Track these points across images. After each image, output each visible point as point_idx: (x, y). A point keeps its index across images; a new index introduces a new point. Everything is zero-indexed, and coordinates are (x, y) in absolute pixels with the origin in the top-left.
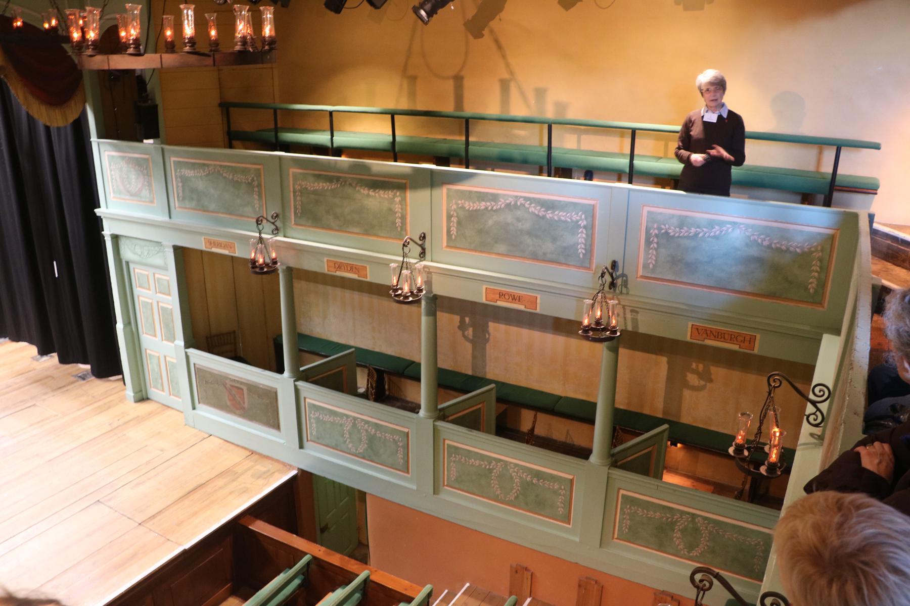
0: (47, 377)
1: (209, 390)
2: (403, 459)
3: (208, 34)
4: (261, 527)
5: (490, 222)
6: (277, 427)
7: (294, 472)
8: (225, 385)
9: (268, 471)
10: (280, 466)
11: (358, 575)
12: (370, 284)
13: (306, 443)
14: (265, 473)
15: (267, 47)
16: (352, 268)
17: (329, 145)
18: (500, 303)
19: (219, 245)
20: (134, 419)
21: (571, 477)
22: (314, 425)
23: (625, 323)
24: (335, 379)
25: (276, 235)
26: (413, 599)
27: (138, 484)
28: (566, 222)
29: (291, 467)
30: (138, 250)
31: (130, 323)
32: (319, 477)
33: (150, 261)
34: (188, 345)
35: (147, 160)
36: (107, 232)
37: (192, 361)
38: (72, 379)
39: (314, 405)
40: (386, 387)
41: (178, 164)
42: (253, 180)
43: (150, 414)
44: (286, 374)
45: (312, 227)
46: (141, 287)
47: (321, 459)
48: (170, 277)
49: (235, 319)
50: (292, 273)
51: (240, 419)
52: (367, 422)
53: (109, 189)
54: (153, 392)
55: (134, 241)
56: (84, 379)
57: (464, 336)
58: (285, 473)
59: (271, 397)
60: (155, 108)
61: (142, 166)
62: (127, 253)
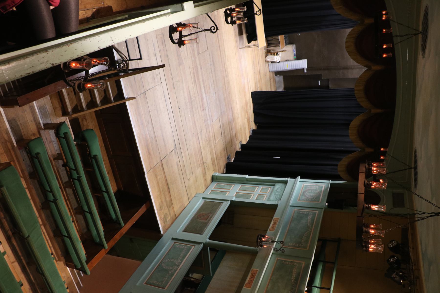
0: (232, 144)
1: (210, 206)
3: (373, 224)
4: (142, 210)
6: (185, 231)
7: (162, 232)
8: (210, 213)
9: (166, 222)
10: (167, 227)
11: (107, 243)
12: (242, 287)
13: (174, 241)
14: (166, 220)
15: (364, 244)
16: (251, 281)
17: (314, 285)
19: (274, 224)
20: (205, 172)
22: (181, 247)
24: (199, 264)
25: (274, 250)
26: (87, 264)
27: (178, 165)
29: (165, 232)
30: (279, 190)
31: (247, 181)
32: (157, 243)
33: (273, 194)
34: (232, 201)
35: (319, 201)
36: (289, 179)
37: (225, 202)
38: (229, 154)
39: (190, 249)
40: (189, 289)
41: (315, 213)
42: (302, 245)
43: (205, 180)
44: (208, 240)
45: (275, 266)
46: (262, 189)
47: (165, 245)
48: (264, 201)
49: (239, 226)
50: (254, 254)
51: (193, 216)
52: (175, 271)
53: (308, 184)
54: (215, 184)
55: (283, 190)
56: (227, 158)
58: (163, 228)
59: (200, 232)
60: (342, 209)
61: (316, 198)
62: (278, 186)
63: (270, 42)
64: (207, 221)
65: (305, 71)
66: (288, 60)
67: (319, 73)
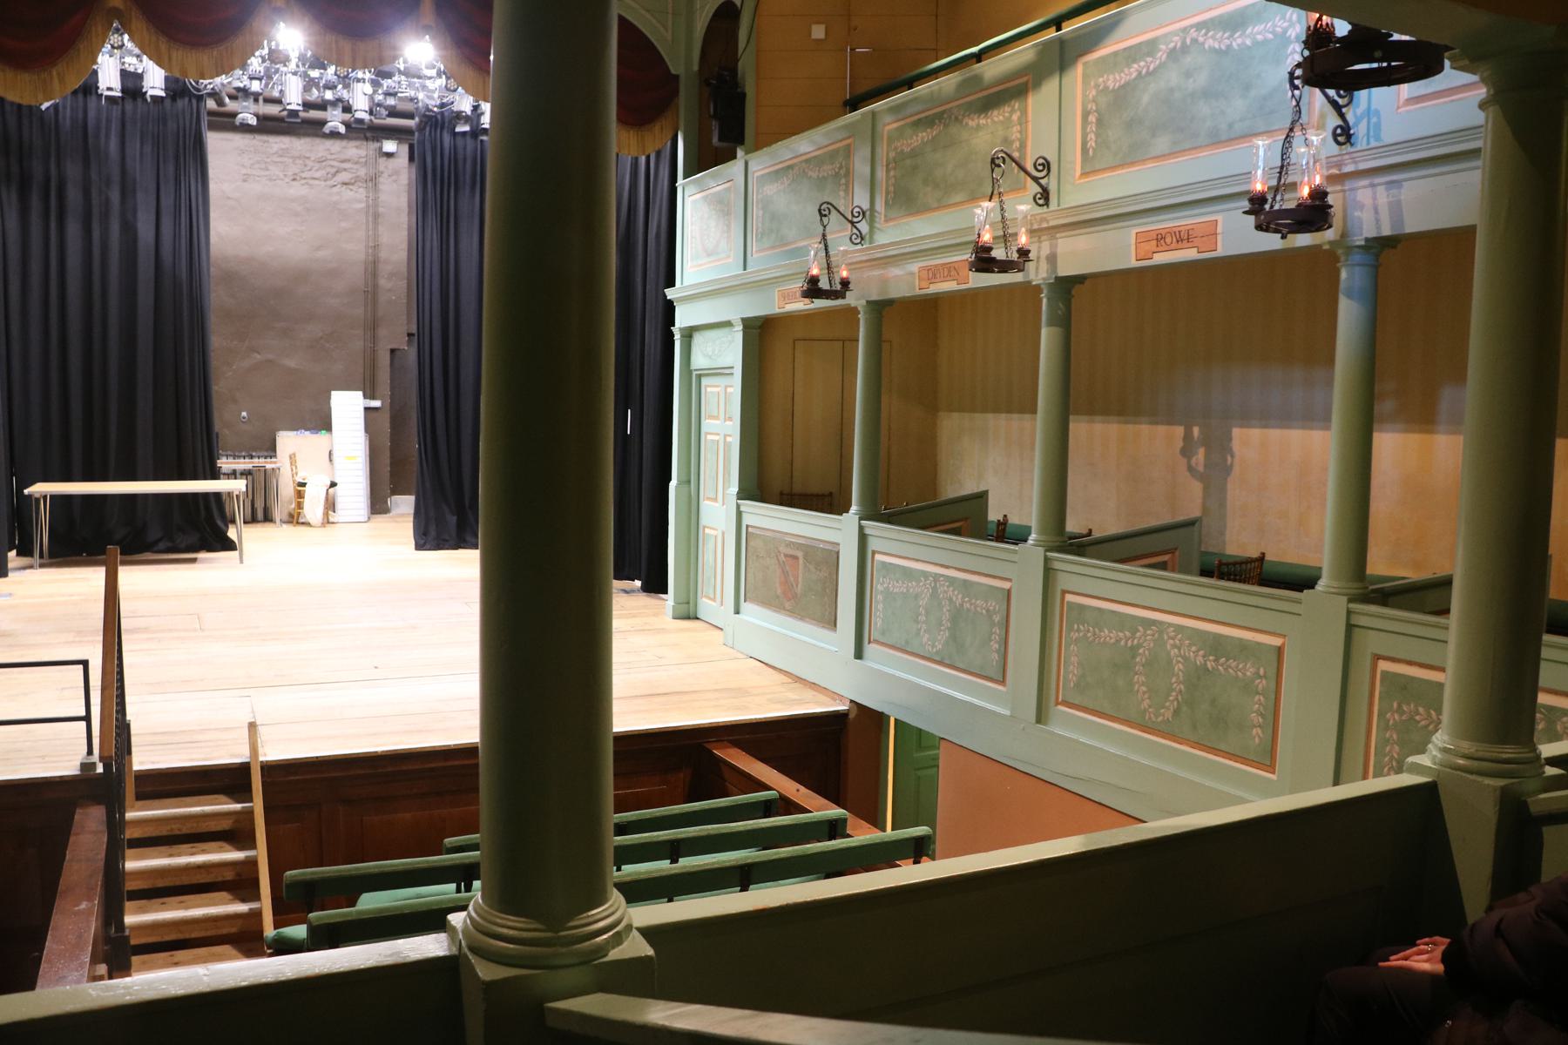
2: (997, 651)
5: (1146, 99)
13: (869, 649)
18: (1161, 258)
21: (1277, 642)
22: (880, 607)
23: (1377, 221)
28: (1265, 42)
34: (745, 493)
57: (1190, 469)
59: (829, 559)
63: (260, 515)
64: (800, 554)
65: (377, 403)
66: (330, 453)
67: (384, 359)
